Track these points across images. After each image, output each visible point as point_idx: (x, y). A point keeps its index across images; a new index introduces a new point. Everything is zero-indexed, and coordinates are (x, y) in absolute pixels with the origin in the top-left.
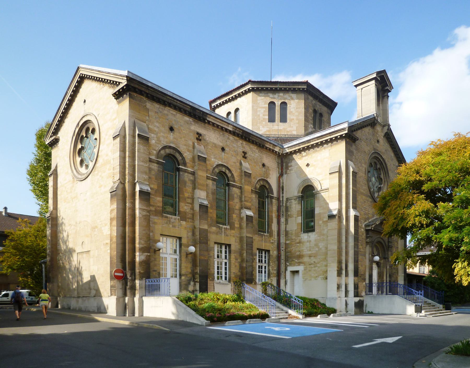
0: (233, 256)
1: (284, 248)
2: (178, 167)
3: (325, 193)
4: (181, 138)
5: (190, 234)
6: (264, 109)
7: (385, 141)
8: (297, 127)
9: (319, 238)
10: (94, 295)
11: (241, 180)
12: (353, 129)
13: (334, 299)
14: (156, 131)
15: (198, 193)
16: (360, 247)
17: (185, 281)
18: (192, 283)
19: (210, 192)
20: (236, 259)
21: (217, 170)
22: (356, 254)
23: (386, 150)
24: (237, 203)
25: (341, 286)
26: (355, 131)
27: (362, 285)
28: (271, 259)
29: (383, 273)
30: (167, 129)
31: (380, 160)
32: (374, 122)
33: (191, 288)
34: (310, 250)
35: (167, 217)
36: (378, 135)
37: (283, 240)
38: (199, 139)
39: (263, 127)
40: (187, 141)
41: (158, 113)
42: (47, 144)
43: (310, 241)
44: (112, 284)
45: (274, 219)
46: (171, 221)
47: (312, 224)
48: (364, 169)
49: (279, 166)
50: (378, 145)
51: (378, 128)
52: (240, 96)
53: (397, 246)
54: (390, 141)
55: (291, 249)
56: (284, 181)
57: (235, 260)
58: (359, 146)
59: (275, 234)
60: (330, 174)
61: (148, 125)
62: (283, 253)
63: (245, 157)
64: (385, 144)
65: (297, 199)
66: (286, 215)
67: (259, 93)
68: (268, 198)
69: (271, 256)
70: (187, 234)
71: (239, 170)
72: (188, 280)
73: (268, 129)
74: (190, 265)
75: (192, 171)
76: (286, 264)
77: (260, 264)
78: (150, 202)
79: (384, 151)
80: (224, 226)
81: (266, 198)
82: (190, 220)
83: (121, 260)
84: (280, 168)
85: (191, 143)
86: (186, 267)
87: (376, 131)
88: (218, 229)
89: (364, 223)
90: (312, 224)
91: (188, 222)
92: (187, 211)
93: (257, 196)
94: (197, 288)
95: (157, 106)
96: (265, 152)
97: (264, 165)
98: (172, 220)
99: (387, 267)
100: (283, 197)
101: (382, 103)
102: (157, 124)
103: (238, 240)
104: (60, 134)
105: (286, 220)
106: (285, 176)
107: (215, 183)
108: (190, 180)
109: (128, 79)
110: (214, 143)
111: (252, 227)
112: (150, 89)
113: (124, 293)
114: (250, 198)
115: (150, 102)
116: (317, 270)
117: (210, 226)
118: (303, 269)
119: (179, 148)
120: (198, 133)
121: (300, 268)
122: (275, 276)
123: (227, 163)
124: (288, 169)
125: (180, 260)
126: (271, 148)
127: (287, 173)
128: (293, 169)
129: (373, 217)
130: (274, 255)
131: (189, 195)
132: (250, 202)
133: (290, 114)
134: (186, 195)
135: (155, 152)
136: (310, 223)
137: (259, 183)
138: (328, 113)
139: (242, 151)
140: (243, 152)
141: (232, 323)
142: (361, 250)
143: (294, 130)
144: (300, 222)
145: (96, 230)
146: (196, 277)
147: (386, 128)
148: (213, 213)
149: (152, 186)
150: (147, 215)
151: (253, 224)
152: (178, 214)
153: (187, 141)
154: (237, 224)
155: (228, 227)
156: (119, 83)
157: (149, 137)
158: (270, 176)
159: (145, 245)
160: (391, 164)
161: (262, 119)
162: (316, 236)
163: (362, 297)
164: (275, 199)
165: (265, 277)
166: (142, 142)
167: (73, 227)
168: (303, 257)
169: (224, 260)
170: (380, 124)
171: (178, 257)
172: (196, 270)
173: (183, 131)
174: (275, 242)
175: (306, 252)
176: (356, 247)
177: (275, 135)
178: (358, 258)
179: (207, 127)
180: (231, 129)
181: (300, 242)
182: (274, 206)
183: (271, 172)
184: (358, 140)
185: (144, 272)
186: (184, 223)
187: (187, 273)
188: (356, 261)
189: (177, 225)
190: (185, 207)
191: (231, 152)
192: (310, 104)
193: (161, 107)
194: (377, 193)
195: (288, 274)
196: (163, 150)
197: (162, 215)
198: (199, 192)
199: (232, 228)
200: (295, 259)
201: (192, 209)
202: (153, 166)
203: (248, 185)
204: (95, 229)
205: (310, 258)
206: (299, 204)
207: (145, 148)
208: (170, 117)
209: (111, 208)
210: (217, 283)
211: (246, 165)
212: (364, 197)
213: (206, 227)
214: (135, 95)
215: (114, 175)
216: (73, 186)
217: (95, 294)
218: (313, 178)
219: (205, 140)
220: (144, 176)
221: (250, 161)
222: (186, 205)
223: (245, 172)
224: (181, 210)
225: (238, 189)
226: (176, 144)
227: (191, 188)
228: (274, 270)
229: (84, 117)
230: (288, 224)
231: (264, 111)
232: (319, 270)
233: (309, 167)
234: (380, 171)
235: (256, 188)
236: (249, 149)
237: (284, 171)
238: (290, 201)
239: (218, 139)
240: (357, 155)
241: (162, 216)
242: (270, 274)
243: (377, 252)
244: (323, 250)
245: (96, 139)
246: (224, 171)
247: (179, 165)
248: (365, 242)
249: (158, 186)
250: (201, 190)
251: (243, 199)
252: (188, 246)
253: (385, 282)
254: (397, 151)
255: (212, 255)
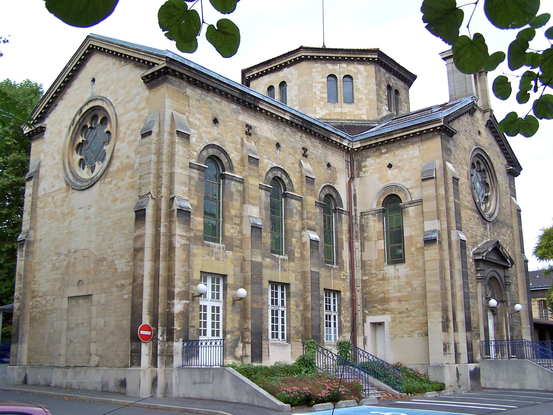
0: (293, 302)
1: (360, 288)
2: (223, 173)
3: (417, 207)
4: (227, 133)
5: (238, 269)
6: (322, 85)
7: (487, 131)
8: (367, 110)
9: (411, 272)
10: (96, 364)
11: (302, 187)
12: (449, 119)
13: (440, 367)
14: (197, 125)
15: (249, 209)
16: (470, 286)
17: (230, 342)
18: (241, 345)
19: (263, 208)
20: (297, 306)
21: (271, 176)
22: (466, 296)
23: (490, 144)
24: (297, 221)
25: (449, 346)
26: (451, 121)
27: (477, 343)
28: (343, 305)
29: (501, 323)
30: (211, 121)
31: (485, 159)
32: (473, 108)
33: (239, 352)
34: (399, 291)
35: (208, 246)
36: (478, 125)
37: (358, 275)
38: (248, 134)
39: (321, 109)
40: (234, 136)
41: (199, 101)
42: (26, 134)
43: (399, 278)
44: (134, 347)
45: (344, 243)
46: (214, 251)
47: (400, 251)
48: (465, 172)
49: (348, 166)
50: (480, 137)
51: (478, 115)
52: (286, 65)
53: (516, 282)
54: (494, 131)
55: (371, 288)
56: (357, 188)
57: (295, 307)
58: (458, 140)
59: (346, 266)
60: (423, 180)
61: (187, 118)
62: (359, 295)
63: (305, 155)
64: (488, 135)
65: (377, 214)
66: (361, 237)
67: (314, 62)
68: (335, 212)
69: (342, 300)
70: (234, 270)
71: (298, 174)
72: (234, 340)
73: (328, 112)
74: (237, 317)
75: (240, 179)
76: (364, 312)
77: (328, 313)
78: (189, 226)
79: (487, 145)
80: (281, 257)
81: (332, 213)
82: (237, 249)
83: (149, 311)
84: (350, 169)
85: (239, 140)
86: (233, 320)
87: (476, 119)
88: (273, 262)
89: (472, 249)
90: (400, 251)
91: (235, 252)
92: (234, 235)
93: (322, 210)
94: (247, 352)
95: (199, 91)
96: (329, 147)
97: (329, 165)
98: (216, 250)
99: (506, 315)
100: (355, 210)
101: (480, 79)
102: (198, 116)
103: (299, 277)
104: (48, 122)
105: (362, 245)
106: (357, 180)
107: (269, 194)
108: (238, 191)
109: (168, 60)
110: (267, 138)
111: (318, 257)
112: (192, 71)
113: (150, 362)
114: (314, 214)
115: (191, 87)
116: (412, 322)
117: (264, 257)
118: (390, 321)
119: (225, 146)
120: (247, 126)
121: (386, 318)
122: (347, 331)
123: (283, 165)
124: (362, 171)
125: (225, 309)
126: (338, 141)
127: (360, 176)
128: (369, 171)
129: (482, 240)
130: (347, 298)
131: (236, 213)
132: (314, 220)
133: (357, 92)
134: (233, 212)
135: (195, 154)
136: (397, 250)
137: (324, 191)
138: (405, 89)
139: (301, 147)
140: (303, 148)
141: (323, 406)
142: (472, 290)
143: (363, 114)
144: (383, 248)
145: (105, 263)
146: (246, 336)
147: (488, 114)
148: (267, 237)
149: (192, 202)
150: (187, 244)
151: (318, 253)
152: (222, 241)
153: (234, 136)
154: (297, 252)
155: (286, 258)
156: (154, 64)
157: (189, 135)
158: (338, 181)
159: (183, 289)
160: (497, 163)
161: (319, 98)
162: (408, 269)
163: (477, 362)
164: (345, 214)
165: (335, 333)
166: (181, 141)
167: (62, 257)
168: (390, 301)
169: (280, 308)
170: (480, 110)
171: (221, 305)
172: (246, 325)
173: (230, 123)
174: (346, 278)
175: (393, 294)
176: (466, 286)
177: (337, 120)
178: (469, 302)
179: (258, 116)
180: (288, 118)
181: (383, 279)
182: (343, 225)
183: (338, 175)
184: (456, 134)
185: (181, 329)
186: (229, 253)
187: (234, 329)
188: (467, 308)
189: (222, 257)
190: (232, 231)
191: (288, 149)
192: (382, 79)
193: (204, 93)
194: (484, 205)
195: (368, 326)
196: (205, 151)
197: (203, 243)
198: (250, 208)
199: (291, 259)
200: (376, 305)
201: (241, 232)
202: (193, 174)
203: (310, 195)
204: (102, 262)
205: (401, 302)
206: (379, 221)
207: (185, 149)
208: (215, 105)
209: (135, 234)
210: (274, 344)
211: (307, 166)
212: (469, 212)
213: (259, 259)
214: (174, 80)
215: (140, 187)
216: (67, 196)
217: (98, 362)
218: (399, 185)
219: (255, 134)
220: (183, 188)
221: (312, 160)
222: (233, 228)
223: (307, 176)
224: (227, 234)
225: (297, 201)
226: (221, 142)
227: (239, 202)
228: (348, 322)
229: (91, 101)
230: (364, 251)
231: (322, 87)
232: (414, 321)
233: (391, 169)
234: (485, 174)
235: (320, 199)
236: (310, 144)
237: (355, 173)
238: (366, 217)
239: (271, 131)
240: (456, 154)
241: (203, 245)
242: (343, 327)
243: (491, 292)
244: (419, 291)
245: (108, 132)
246: (279, 176)
247: (224, 170)
248: (475, 279)
249: (198, 202)
250: (253, 205)
251: (305, 216)
252: (236, 289)
253: (505, 339)
254: (504, 145)
255: (265, 300)
